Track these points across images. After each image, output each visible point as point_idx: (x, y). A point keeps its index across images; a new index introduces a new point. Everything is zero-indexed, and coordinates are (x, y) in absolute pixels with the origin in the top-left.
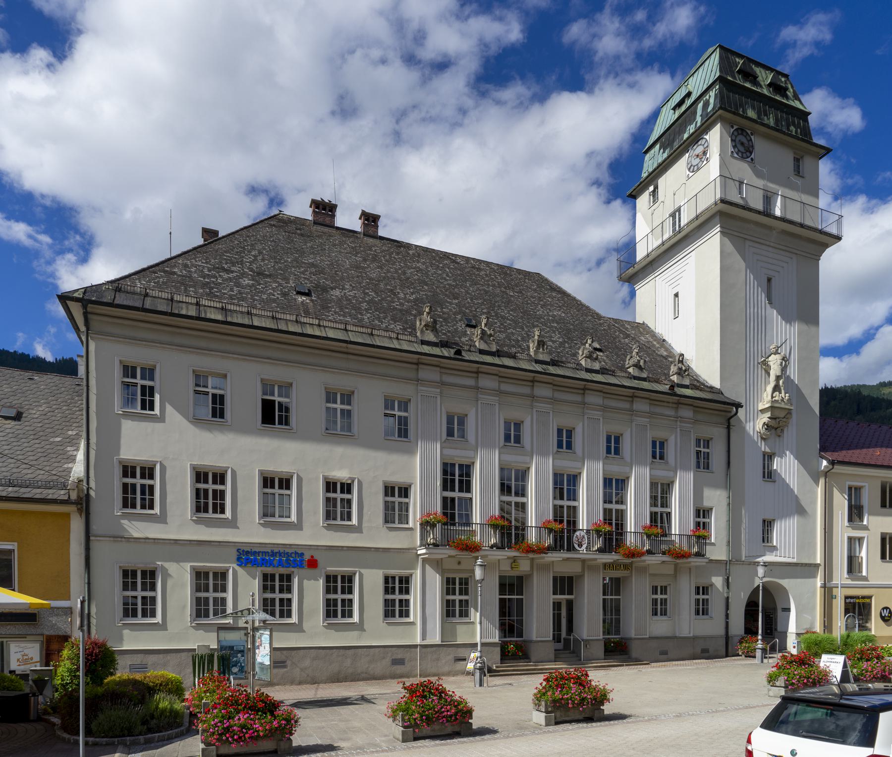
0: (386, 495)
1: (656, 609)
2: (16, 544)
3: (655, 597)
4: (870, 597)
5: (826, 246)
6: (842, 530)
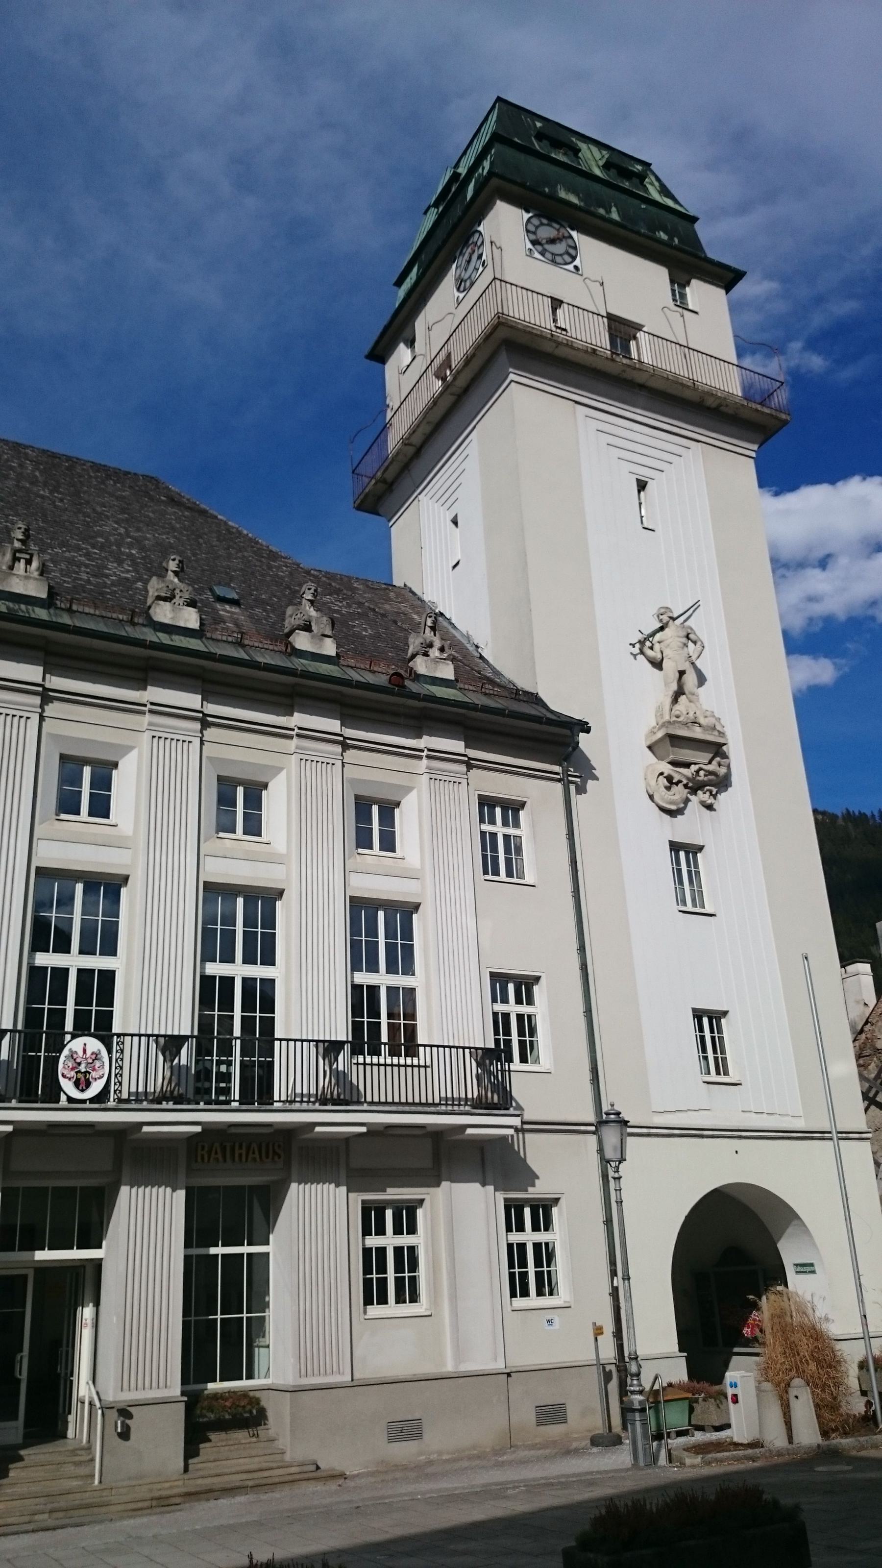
3: (516, 1237)
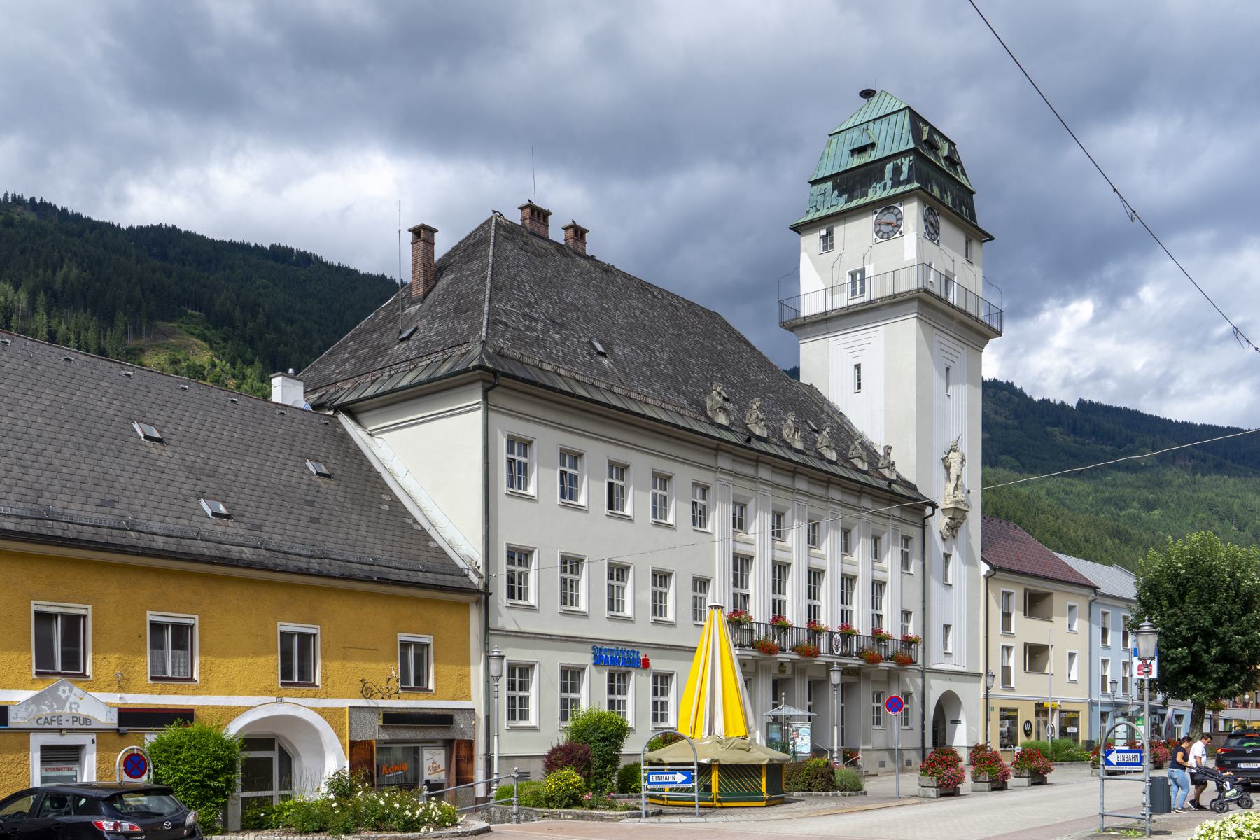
0: (564, 570)
1: (521, 705)
2: (90, 607)
4: (1016, 710)
5: (987, 338)
6: (998, 640)
